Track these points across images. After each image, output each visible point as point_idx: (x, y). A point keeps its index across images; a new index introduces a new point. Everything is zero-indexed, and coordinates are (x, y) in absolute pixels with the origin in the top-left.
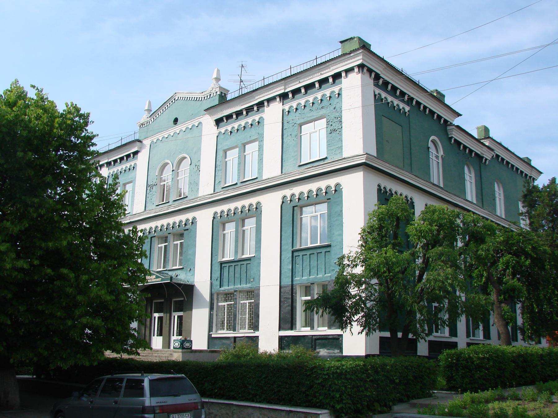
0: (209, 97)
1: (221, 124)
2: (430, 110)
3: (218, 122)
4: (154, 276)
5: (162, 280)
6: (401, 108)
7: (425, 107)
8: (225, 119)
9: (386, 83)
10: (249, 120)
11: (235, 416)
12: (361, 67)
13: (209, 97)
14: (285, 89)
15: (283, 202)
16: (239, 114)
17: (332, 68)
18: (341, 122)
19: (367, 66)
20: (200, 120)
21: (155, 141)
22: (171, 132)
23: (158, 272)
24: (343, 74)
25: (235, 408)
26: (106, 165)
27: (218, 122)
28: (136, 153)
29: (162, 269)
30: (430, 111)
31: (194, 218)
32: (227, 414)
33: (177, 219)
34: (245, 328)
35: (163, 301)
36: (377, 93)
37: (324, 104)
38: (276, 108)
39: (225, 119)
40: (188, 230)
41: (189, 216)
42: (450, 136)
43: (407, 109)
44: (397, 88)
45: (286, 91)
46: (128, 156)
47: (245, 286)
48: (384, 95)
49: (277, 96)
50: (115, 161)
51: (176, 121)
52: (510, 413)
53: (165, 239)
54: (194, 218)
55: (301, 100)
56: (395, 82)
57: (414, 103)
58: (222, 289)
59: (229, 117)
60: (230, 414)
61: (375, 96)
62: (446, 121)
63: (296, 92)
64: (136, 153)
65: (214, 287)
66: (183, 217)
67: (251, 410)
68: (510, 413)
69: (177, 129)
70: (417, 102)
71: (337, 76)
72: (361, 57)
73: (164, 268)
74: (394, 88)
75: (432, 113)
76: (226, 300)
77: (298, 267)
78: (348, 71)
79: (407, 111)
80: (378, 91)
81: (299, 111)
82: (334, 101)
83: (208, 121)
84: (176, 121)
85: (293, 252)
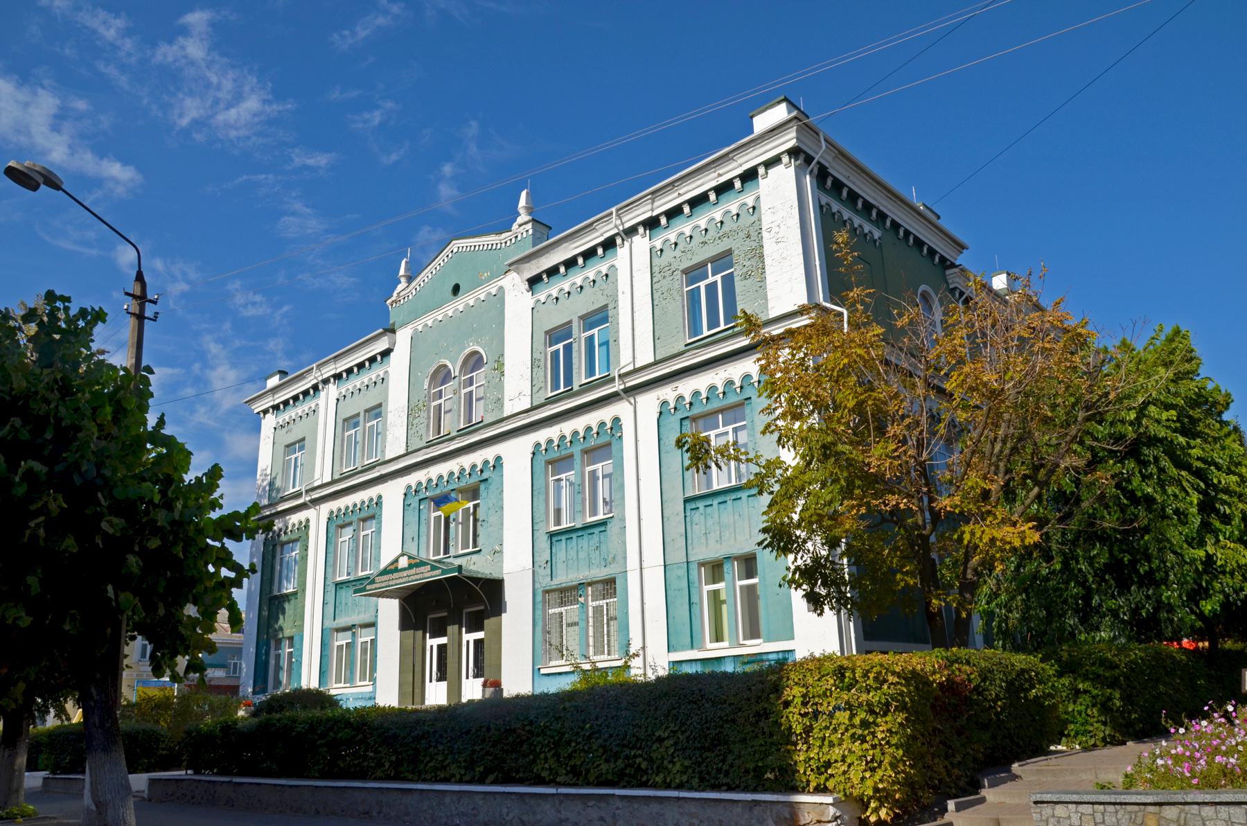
1: (538, 286)
3: (534, 282)
4: (429, 567)
5: (444, 572)
6: (866, 231)
7: (907, 233)
10: (591, 273)
11: (620, 823)
12: (794, 152)
14: (652, 210)
16: (570, 263)
17: (740, 161)
18: (762, 256)
19: (805, 152)
20: (499, 284)
21: (420, 328)
24: (761, 170)
25: (619, 804)
28: (386, 353)
30: (916, 239)
31: (498, 458)
32: (602, 819)
33: (466, 461)
34: (603, 653)
36: (823, 203)
38: (641, 242)
43: (877, 234)
44: (859, 196)
45: (655, 214)
46: (372, 360)
47: (600, 573)
48: (836, 207)
51: (456, 290)
60: (609, 819)
61: (821, 207)
64: (386, 353)
65: (539, 578)
66: (477, 457)
67: (655, 807)
69: (460, 303)
71: (750, 176)
72: (794, 134)
74: (853, 196)
75: (919, 243)
78: (769, 164)
80: (825, 199)
81: (680, 247)
82: (746, 220)
83: (514, 284)
84: (456, 290)
85: (687, 501)
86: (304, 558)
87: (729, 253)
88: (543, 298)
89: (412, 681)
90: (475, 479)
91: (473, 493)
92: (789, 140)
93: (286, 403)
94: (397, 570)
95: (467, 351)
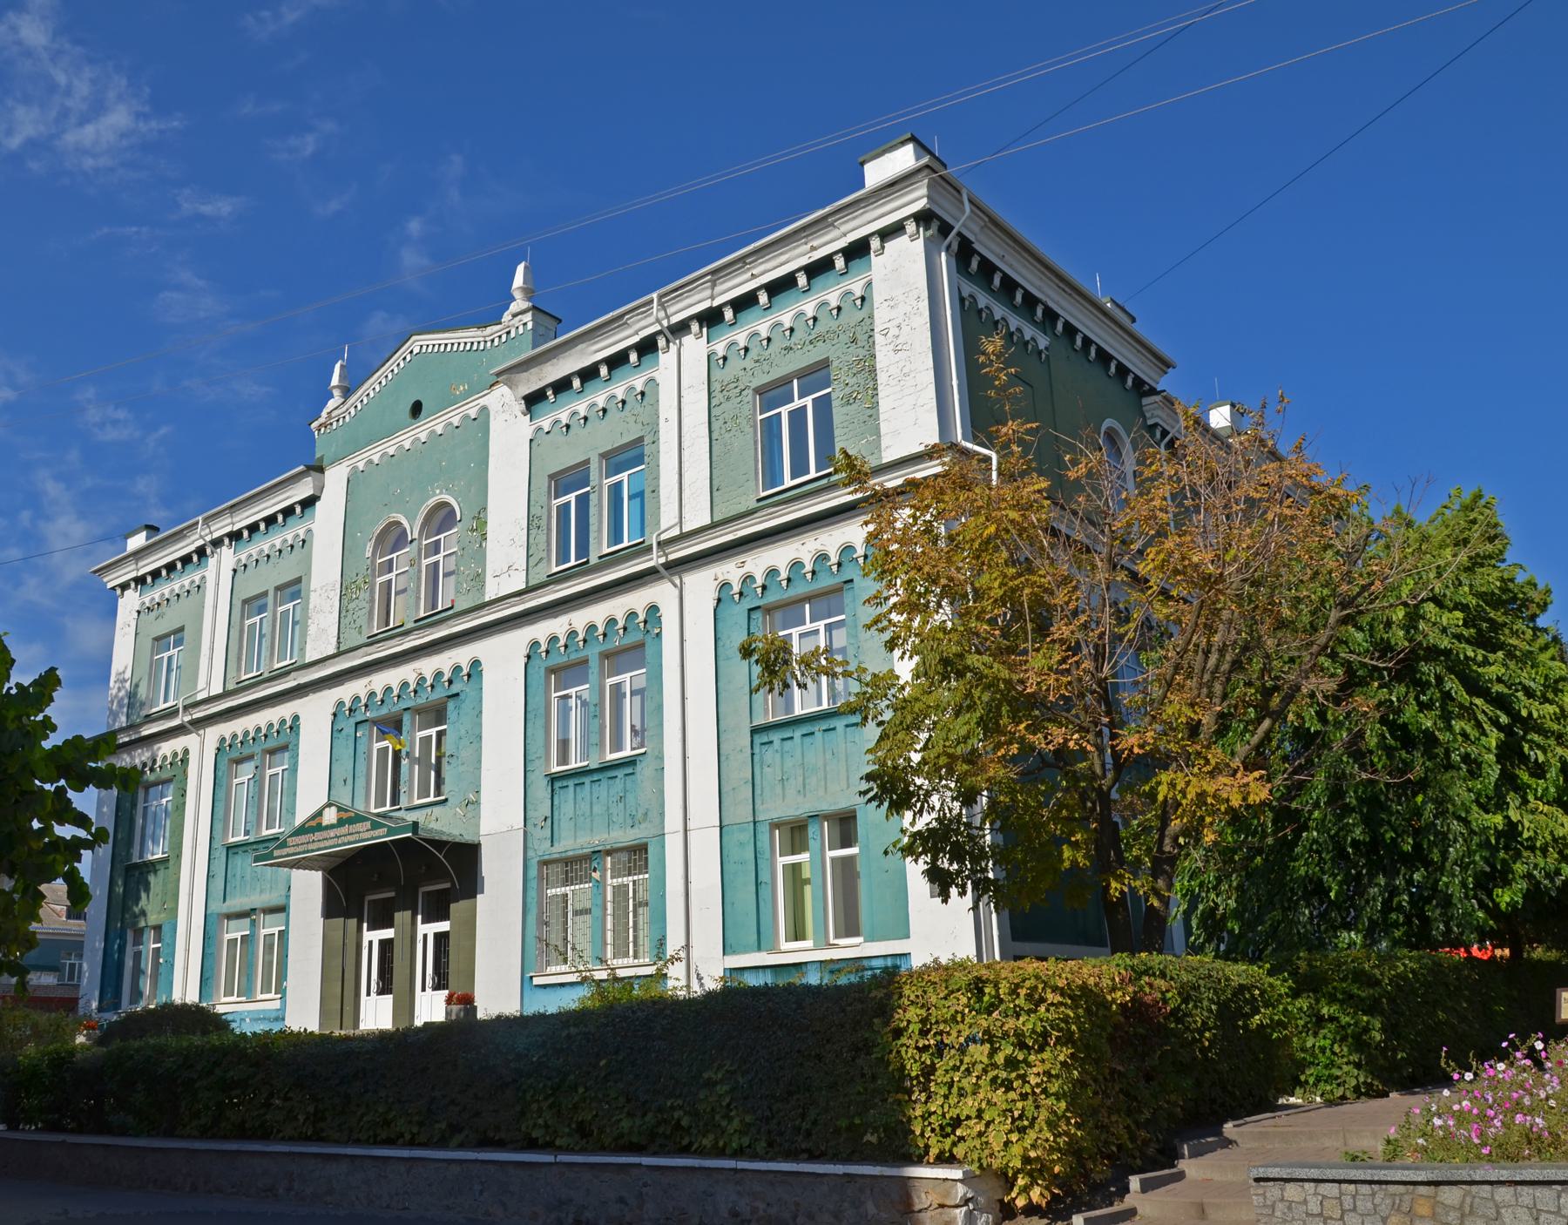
0: (504, 338)
2: (1100, 350)
3: (533, 401)
5: (391, 831)
7: (1087, 342)
8: (549, 393)
9: (987, 268)
12: (923, 218)
13: (504, 338)
14: (713, 298)
15: (719, 600)
17: (844, 228)
20: (482, 402)
22: (406, 439)
23: (378, 815)
24: (875, 243)
26: (227, 541)
27: (533, 401)
28: (309, 503)
29: (388, 808)
31: (476, 663)
33: (427, 666)
34: (626, 955)
35: (392, 894)
36: (965, 295)
37: (821, 328)
38: (695, 346)
39: (549, 393)
40: (457, 695)
41: (461, 656)
42: (1150, 422)
43: (1043, 342)
45: (716, 303)
46: (288, 512)
48: (983, 300)
49: (691, 318)
50: (253, 528)
52: (43, 888)
53: (392, 725)
54: (476, 663)
55: (760, 324)
56: (1011, 266)
57: (1060, 327)
58: (554, 850)
59: (562, 386)
61: (962, 300)
62: (1139, 382)
63: (744, 303)
64: (309, 503)
66: (443, 662)
68: (43, 888)
69: (422, 430)
70: (1067, 325)
71: (858, 251)
72: (924, 191)
73: (393, 804)
75: (1104, 357)
76: (567, 881)
77: (769, 775)
79: (1041, 347)
80: (968, 289)
82: (851, 316)
83: (503, 402)
84: (416, 409)
86: (180, 807)
87: (824, 364)
88: (546, 425)
89: (340, 991)
90: (440, 693)
91: (436, 713)
92: (917, 199)
93: (156, 574)
94: (319, 828)
95: (432, 502)
